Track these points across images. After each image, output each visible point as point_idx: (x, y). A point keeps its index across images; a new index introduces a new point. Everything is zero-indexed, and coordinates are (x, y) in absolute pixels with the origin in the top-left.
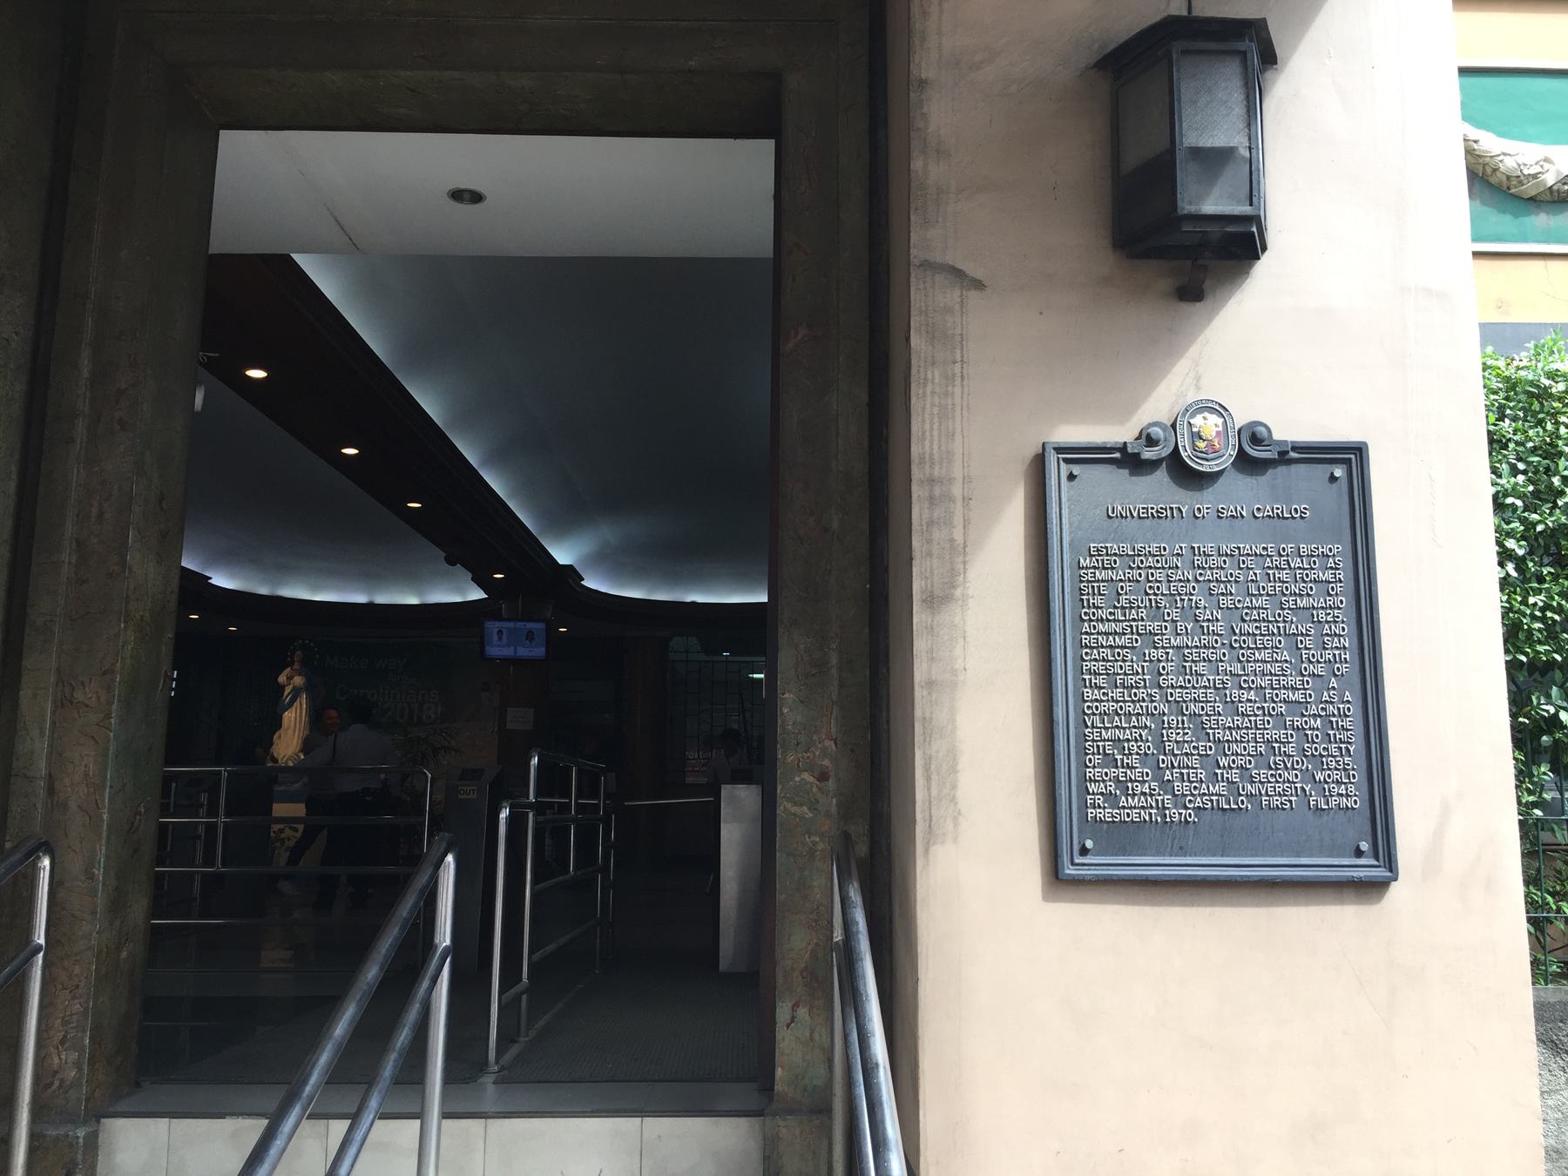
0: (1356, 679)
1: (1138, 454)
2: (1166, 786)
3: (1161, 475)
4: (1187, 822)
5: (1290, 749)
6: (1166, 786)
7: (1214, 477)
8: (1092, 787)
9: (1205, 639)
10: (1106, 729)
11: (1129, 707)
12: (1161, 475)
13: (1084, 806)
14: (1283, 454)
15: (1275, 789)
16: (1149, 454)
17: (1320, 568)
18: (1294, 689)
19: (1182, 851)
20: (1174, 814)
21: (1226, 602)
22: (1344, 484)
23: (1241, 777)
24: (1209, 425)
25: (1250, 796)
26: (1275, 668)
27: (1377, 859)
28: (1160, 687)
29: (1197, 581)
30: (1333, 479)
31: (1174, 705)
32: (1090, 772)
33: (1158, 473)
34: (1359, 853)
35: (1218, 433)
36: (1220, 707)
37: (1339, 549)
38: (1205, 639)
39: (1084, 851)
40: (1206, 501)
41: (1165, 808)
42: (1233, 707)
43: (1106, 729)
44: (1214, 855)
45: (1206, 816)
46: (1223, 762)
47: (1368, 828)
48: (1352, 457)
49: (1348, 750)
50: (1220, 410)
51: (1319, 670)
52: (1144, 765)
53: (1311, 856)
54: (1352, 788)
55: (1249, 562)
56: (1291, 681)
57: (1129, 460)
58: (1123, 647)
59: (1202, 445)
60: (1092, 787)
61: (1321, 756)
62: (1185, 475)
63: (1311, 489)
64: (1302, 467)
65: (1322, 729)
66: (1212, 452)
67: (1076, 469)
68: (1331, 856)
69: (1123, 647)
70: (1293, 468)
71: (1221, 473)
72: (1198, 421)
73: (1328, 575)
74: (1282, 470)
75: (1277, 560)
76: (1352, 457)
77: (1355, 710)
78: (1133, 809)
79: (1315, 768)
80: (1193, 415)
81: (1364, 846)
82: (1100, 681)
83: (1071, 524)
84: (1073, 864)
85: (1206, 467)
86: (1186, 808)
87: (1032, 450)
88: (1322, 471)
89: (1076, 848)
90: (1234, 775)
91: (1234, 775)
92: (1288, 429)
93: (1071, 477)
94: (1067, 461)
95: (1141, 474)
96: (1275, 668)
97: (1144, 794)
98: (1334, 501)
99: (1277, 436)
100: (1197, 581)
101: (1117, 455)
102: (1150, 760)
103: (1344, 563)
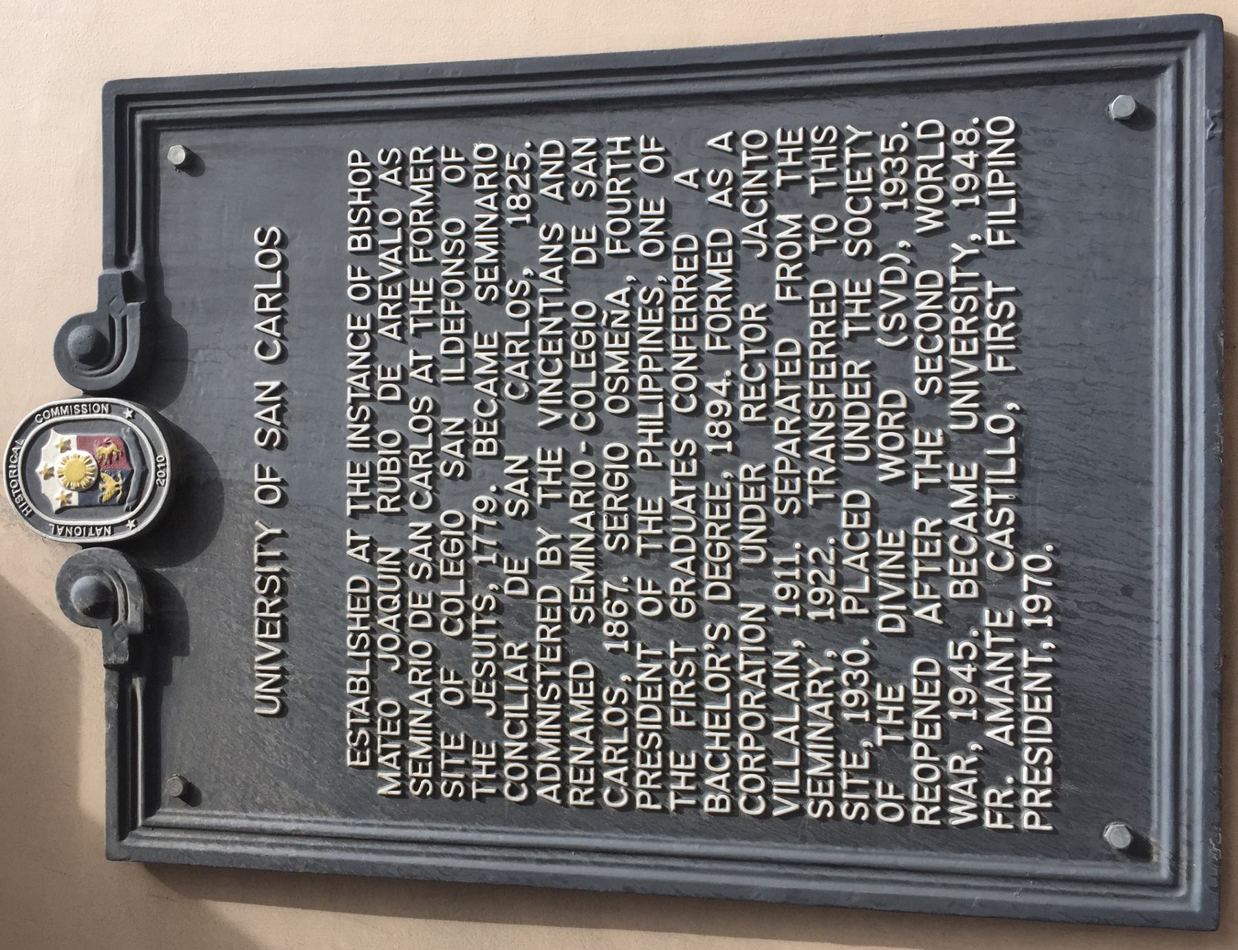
0: (675, 118)
1: (134, 639)
2: (958, 619)
3: (186, 579)
4: (1053, 573)
5: (857, 295)
6: (958, 619)
7: (188, 460)
8: (961, 813)
9: (578, 496)
10: (805, 763)
11: (750, 701)
12: (186, 579)
13: (1015, 842)
14: (130, 288)
15: (966, 333)
16: (132, 614)
17: (403, 203)
18: (701, 278)
19: (1136, 587)
20: (1033, 605)
21: (484, 440)
22: (203, 139)
23: (931, 422)
24: (63, 464)
25: (983, 403)
26: (649, 325)
27: (1159, 69)
28: (698, 617)
29: (434, 509)
30: (192, 165)
31: (744, 585)
32: (578, 798)
33: (180, 586)
34: (1142, 119)
35: (82, 444)
36: (748, 469)
37: (355, 155)
38: (578, 496)
39: (1139, 850)
40: (248, 478)
41: (1018, 627)
42: (750, 437)
43: (805, 763)
44: (1147, 505)
45: (1039, 519)
46: (890, 468)
47: (1070, 94)
48: (143, 125)
49: (858, 144)
50: (30, 436)
51: (653, 215)
52: (897, 673)
53: (1147, 248)
54: (960, 135)
55: (385, 380)
56: (680, 286)
57: (150, 657)
58: (598, 705)
59: (109, 485)
60: (961, 813)
61: (875, 210)
62: (189, 511)
63: (217, 218)
64: (166, 239)
65: (805, 208)
66: (127, 454)
67: (172, 786)
68: (1148, 193)
69: (598, 705)
70: (169, 259)
71: (177, 439)
72: (54, 491)
73: (420, 186)
74: (173, 289)
75: (385, 310)
76: (143, 125)
77: (755, 126)
78: (1019, 709)
79: (907, 232)
80: (44, 503)
81: (1121, 105)
82: (682, 770)
83: (300, 808)
84: (1174, 884)
85: (161, 478)
86: (1016, 571)
87: (139, 883)
88: (176, 194)
89: (1125, 871)
90: (927, 442)
91: (927, 442)
92: (73, 271)
93: (190, 796)
94: (152, 805)
95: (184, 626)
96: (649, 325)
97: (979, 678)
98: (245, 165)
99: (88, 302)
100: (434, 509)
101: (137, 684)
102: (888, 655)
103: (396, 140)
